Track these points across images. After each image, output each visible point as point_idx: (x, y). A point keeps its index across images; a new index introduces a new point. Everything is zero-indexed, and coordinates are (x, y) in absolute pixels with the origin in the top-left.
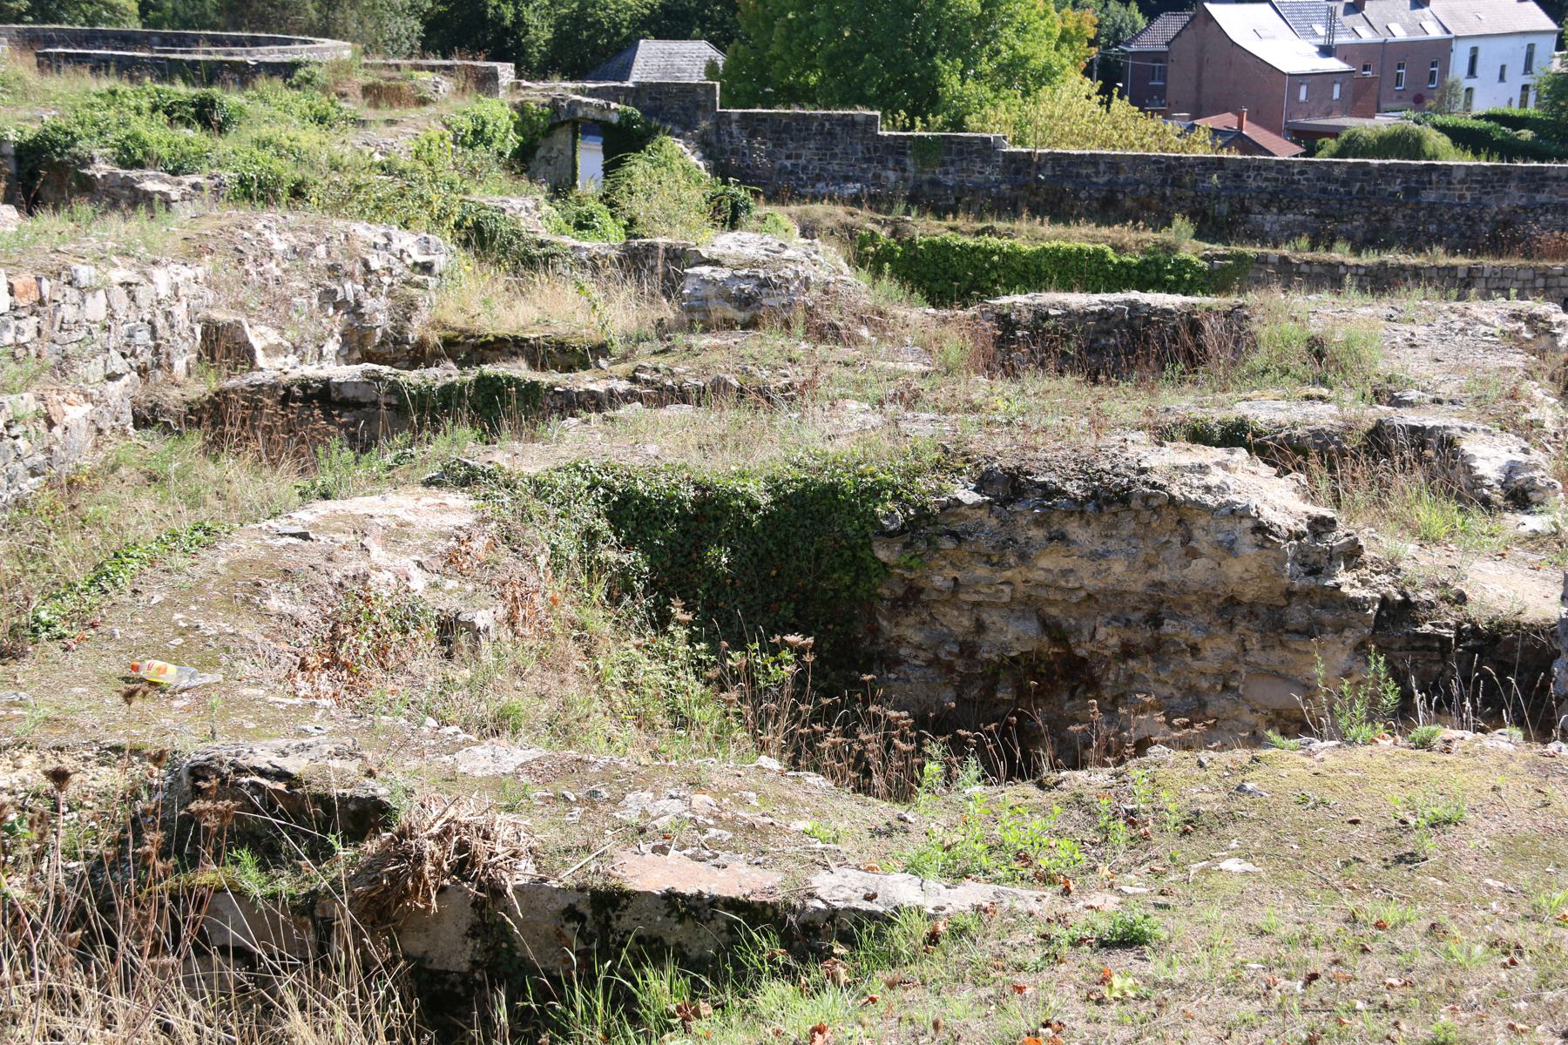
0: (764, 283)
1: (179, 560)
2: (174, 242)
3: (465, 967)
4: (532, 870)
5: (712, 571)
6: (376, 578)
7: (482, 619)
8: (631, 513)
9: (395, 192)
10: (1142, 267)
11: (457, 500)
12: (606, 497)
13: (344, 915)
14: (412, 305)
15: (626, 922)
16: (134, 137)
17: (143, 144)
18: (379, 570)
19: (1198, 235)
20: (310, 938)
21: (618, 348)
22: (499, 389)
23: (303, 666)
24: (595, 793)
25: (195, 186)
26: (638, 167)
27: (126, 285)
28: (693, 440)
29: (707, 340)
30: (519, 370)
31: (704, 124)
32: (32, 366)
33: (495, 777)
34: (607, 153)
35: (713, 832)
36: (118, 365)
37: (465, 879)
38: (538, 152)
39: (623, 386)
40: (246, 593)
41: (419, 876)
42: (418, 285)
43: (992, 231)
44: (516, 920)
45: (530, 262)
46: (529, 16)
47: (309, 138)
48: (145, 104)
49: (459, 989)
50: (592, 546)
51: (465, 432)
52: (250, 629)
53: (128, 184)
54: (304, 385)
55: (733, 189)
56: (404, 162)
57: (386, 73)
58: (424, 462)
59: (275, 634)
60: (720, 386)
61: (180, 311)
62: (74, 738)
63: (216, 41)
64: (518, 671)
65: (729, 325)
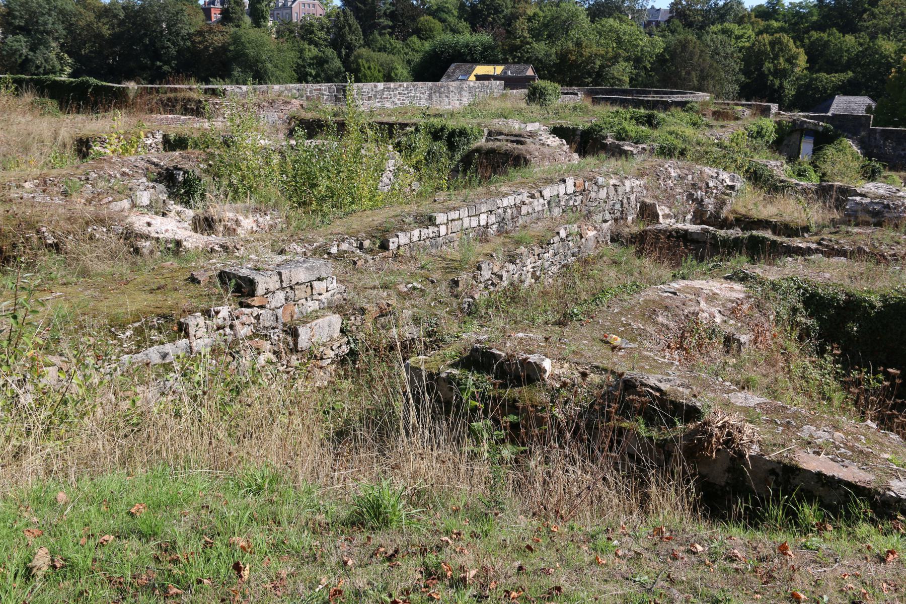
0: (887, 206)
1: (626, 297)
2: (634, 170)
3: (723, 484)
4: (758, 450)
5: (848, 332)
6: (701, 315)
7: (744, 338)
8: (814, 302)
9: (722, 156)
11: (738, 286)
12: (804, 294)
13: (678, 450)
14: (724, 203)
15: (797, 481)
16: (623, 129)
17: (626, 131)
18: (703, 311)
20: (663, 457)
21: (814, 229)
22: (757, 242)
23: (669, 347)
24: (789, 423)
25: (643, 149)
26: (830, 151)
27: (614, 185)
28: (847, 273)
29: (856, 230)
30: (768, 234)
31: (863, 133)
32: (578, 214)
33: (745, 407)
34: (815, 144)
35: (843, 450)
36: (608, 216)
37: (729, 447)
38: (785, 142)
39: (814, 246)
40: (649, 312)
41: (710, 442)
42: (727, 195)
44: (748, 469)
45: (776, 189)
46: (786, 84)
47: (689, 131)
48: (628, 116)
49: (719, 492)
50: (794, 314)
51: (744, 258)
52: (650, 328)
53: (619, 146)
54: (677, 231)
55: (874, 163)
56: (727, 143)
57: (723, 107)
58: (726, 269)
59: (659, 332)
60: (860, 250)
61: (633, 198)
62: (582, 360)
63: (657, 93)
64: (755, 364)
65: (867, 224)
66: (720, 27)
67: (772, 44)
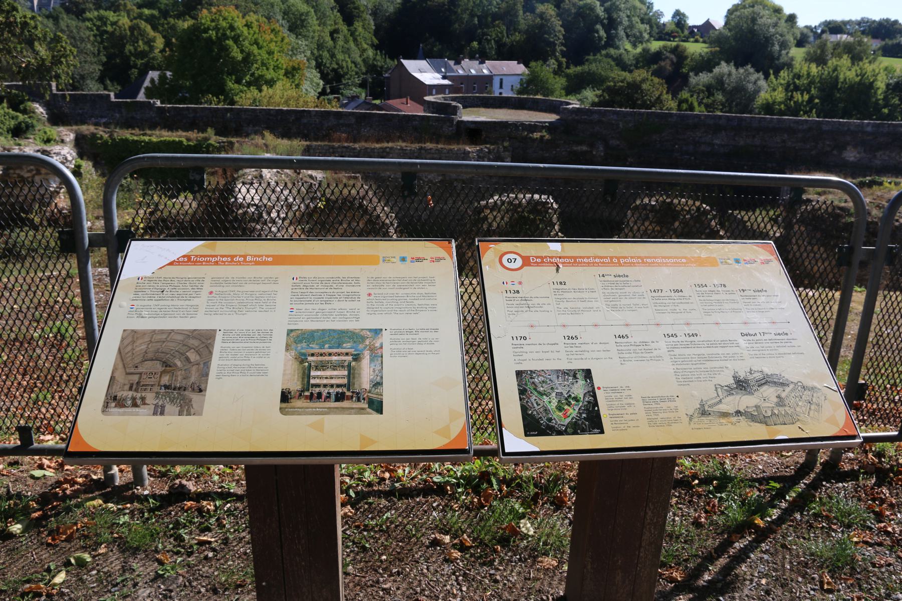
10: (195, 146)
19: (216, 135)
43: (144, 135)
66: (96, 13)
67: (132, 29)
